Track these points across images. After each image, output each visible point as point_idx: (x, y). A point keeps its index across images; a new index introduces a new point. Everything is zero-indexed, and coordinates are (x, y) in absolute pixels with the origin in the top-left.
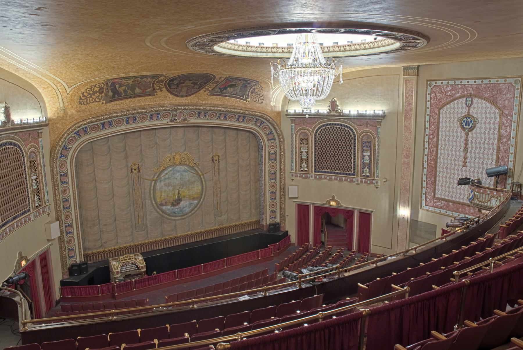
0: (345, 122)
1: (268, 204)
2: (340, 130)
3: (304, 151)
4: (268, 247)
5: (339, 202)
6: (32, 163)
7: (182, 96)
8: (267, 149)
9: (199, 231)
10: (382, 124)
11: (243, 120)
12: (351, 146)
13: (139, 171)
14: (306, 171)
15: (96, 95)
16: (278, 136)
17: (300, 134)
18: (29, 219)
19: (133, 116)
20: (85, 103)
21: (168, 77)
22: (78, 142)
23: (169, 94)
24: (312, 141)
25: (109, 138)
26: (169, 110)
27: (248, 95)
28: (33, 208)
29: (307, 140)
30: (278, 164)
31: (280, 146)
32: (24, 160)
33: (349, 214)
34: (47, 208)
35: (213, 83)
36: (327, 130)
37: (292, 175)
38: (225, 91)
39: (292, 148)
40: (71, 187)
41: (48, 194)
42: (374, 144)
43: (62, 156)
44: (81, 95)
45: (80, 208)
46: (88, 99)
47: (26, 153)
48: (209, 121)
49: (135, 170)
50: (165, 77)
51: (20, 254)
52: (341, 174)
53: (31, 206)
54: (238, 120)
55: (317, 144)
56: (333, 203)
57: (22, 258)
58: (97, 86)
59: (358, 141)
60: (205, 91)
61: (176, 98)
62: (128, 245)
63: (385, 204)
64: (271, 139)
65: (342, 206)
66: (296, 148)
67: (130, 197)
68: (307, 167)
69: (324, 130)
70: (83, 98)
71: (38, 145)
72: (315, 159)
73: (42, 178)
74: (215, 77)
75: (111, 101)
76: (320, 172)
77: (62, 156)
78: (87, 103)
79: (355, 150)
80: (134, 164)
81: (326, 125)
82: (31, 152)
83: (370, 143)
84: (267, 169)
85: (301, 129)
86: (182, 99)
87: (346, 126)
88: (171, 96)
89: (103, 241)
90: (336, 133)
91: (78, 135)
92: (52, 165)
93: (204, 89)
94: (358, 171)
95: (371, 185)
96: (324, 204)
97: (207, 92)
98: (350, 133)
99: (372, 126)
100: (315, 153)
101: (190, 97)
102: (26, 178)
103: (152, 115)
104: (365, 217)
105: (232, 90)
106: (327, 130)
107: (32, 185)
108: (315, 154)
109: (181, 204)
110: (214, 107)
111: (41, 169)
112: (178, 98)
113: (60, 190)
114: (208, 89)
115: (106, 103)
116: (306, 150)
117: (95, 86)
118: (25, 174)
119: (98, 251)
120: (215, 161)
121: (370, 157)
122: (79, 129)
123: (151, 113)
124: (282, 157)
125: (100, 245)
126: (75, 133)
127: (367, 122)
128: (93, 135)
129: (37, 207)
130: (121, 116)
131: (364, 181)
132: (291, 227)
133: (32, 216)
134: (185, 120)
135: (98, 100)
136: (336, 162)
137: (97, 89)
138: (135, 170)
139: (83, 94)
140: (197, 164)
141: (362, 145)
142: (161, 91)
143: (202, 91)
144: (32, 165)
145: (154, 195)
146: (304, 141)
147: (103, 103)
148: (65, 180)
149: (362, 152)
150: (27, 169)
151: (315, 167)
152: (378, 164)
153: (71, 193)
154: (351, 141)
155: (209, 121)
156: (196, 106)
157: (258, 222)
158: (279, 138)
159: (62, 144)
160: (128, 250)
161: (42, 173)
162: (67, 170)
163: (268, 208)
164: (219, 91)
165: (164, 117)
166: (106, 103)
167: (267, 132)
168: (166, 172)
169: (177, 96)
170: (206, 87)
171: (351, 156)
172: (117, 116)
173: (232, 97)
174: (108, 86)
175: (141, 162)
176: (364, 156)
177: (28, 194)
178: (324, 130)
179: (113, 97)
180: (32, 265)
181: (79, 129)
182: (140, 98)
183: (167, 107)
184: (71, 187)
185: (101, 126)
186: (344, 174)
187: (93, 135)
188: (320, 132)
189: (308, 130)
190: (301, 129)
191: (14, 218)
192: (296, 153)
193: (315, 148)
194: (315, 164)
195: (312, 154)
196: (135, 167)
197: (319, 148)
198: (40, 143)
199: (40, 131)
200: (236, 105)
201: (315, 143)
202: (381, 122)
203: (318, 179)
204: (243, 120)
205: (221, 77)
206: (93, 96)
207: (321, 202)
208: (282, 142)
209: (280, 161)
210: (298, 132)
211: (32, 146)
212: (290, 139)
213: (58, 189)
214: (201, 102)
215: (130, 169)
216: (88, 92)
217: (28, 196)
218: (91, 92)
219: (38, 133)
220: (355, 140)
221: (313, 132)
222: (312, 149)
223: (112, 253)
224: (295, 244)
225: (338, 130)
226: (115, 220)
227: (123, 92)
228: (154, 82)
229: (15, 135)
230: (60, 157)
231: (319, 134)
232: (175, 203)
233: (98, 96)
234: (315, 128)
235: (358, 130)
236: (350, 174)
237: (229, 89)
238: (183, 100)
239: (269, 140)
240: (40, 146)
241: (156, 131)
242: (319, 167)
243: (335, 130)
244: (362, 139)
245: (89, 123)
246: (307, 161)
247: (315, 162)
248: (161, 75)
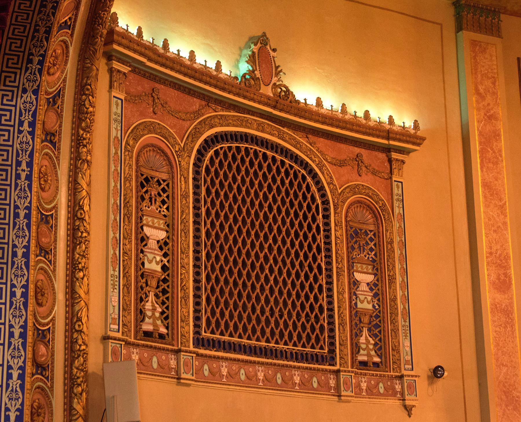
3: (156, 234)
176: (356, 283)
246: (165, 288)
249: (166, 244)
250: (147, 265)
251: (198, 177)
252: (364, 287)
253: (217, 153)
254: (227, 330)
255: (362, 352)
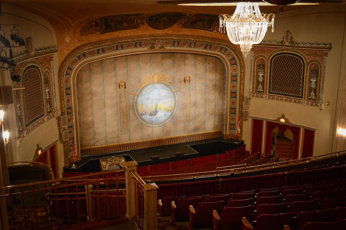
0: (297, 52)
1: (228, 117)
2: (292, 59)
3: (261, 75)
4: (225, 152)
5: (287, 119)
6: (46, 80)
7: (160, 29)
8: (230, 72)
9: (182, 135)
10: (328, 54)
11: (210, 47)
12: (300, 72)
13: (125, 87)
14: (261, 92)
15: (93, 28)
16: (240, 62)
17: (258, 60)
18: (44, 121)
19: (121, 44)
20: (85, 34)
21: (148, 15)
22: (79, 64)
23: (149, 27)
24: (267, 67)
25: (103, 61)
26: (149, 40)
27: (215, 27)
28: (46, 113)
29: (264, 66)
30: (238, 85)
31: (241, 70)
32: (41, 78)
33: (296, 130)
34: (56, 113)
35: (185, 19)
36: (281, 58)
37: (250, 95)
38: (195, 24)
39: (251, 72)
40: (73, 98)
41: (57, 104)
42: (321, 72)
43: (67, 74)
44: (82, 28)
45: (79, 114)
46: (87, 31)
47: (42, 73)
48: (182, 48)
49: (122, 86)
50: (146, 15)
51: (38, 145)
52: (291, 96)
53: (45, 111)
54: (206, 48)
55: (272, 70)
56: (283, 120)
57: (39, 148)
58: (94, 21)
59: (307, 69)
60: (178, 25)
61: (155, 30)
62: (114, 144)
63: (326, 124)
64: (234, 64)
65: (290, 123)
66: (254, 72)
67: (117, 107)
68: (263, 88)
69: (279, 58)
70: (83, 30)
71: (50, 66)
72: (270, 82)
73: (53, 91)
74: (186, 15)
75: (104, 33)
76: (273, 93)
77: (67, 74)
78: (86, 34)
79: (303, 76)
80: (122, 82)
81: (280, 54)
82: (46, 71)
83: (317, 71)
84: (229, 89)
85: (259, 56)
86: (160, 31)
87: (297, 56)
88: (151, 29)
89: (96, 141)
90: (289, 61)
91: (79, 58)
92: (59, 81)
93: (178, 23)
94: (305, 94)
95: (316, 107)
96: (275, 120)
97: (180, 25)
98: (300, 62)
99: (320, 56)
100: (270, 77)
101: (166, 29)
102: (42, 91)
103: (136, 43)
104: (310, 134)
105: (201, 23)
106: (281, 58)
107: (46, 96)
108: (270, 78)
109: (157, 115)
110: (186, 38)
111: (52, 84)
112: (157, 30)
113: (65, 100)
114: (180, 23)
115: (100, 34)
116: (263, 75)
117: (92, 21)
118: (42, 88)
119: (91, 147)
120: (186, 81)
121: (316, 83)
122: (79, 54)
123: (135, 42)
124: (242, 79)
125: (93, 143)
126: (77, 57)
127: (316, 52)
128: (90, 58)
129: (49, 112)
130: (112, 44)
131: (310, 103)
132: (247, 139)
133: (45, 119)
134: (162, 47)
135: (95, 32)
136: (287, 85)
137: (94, 24)
138: (122, 86)
139: (83, 27)
140: (172, 83)
141: (310, 72)
142: (143, 25)
143: (176, 25)
144: (46, 81)
145: (136, 106)
146: (261, 67)
147: (98, 34)
148: (69, 93)
149: (310, 78)
150: (43, 85)
151: (269, 89)
152: (323, 89)
153: (73, 102)
154: (301, 68)
155: (182, 48)
156: (171, 36)
157: (220, 133)
158: (240, 64)
159: (67, 66)
160: (114, 148)
161: (52, 87)
162: (71, 85)
163: (228, 121)
164: (190, 24)
165: (146, 45)
166: (100, 34)
167: (230, 58)
168: (146, 89)
169: (156, 28)
170: (179, 21)
171: (300, 81)
172: (109, 44)
173: (201, 29)
174: (102, 21)
175: (127, 80)
176: (311, 82)
177: (43, 103)
178: (279, 58)
179: (106, 29)
180: (44, 154)
181: (79, 54)
182: (127, 31)
183: (148, 37)
184: (73, 98)
185: (96, 52)
186: (293, 96)
187: (90, 58)
188: (275, 59)
189: (265, 57)
190: (259, 56)
191: (35, 120)
192: (254, 76)
193: (270, 73)
194: (270, 86)
195: (267, 77)
196: (122, 84)
197: (273, 73)
198: (52, 65)
199: (52, 56)
200: (205, 35)
201: (271, 69)
202: (327, 53)
203: (271, 99)
204: (210, 47)
205: (191, 15)
206: (91, 29)
207: (272, 118)
208: (243, 67)
209: (240, 82)
210: (256, 59)
211: (46, 67)
212: (250, 65)
213: (64, 99)
214: (175, 33)
215: (119, 85)
216: (87, 26)
217: (43, 104)
218: (89, 26)
219: (51, 57)
220: (304, 68)
221: (269, 59)
222: (267, 73)
223: (102, 150)
224: (249, 152)
225: (290, 59)
226: (106, 125)
227: (113, 26)
228: (138, 18)
229: (35, 60)
230: (66, 75)
231: (274, 61)
232: (152, 114)
233: (95, 29)
234: (271, 55)
235: (307, 59)
236: (298, 97)
237: (198, 23)
238: (160, 32)
239: (231, 65)
240: (52, 67)
241: (140, 55)
242: (272, 89)
243: (288, 58)
244: (310, 67)
245: (87, 50)
246: (263, 83)
247: (270, 85)
248: (143, 14)
249: (264, 76)
250: (259, 80)
251: (82, 57)
252: (313, 82)
253: (276, 58)
254: (283, 91)
255: (311, 96)
